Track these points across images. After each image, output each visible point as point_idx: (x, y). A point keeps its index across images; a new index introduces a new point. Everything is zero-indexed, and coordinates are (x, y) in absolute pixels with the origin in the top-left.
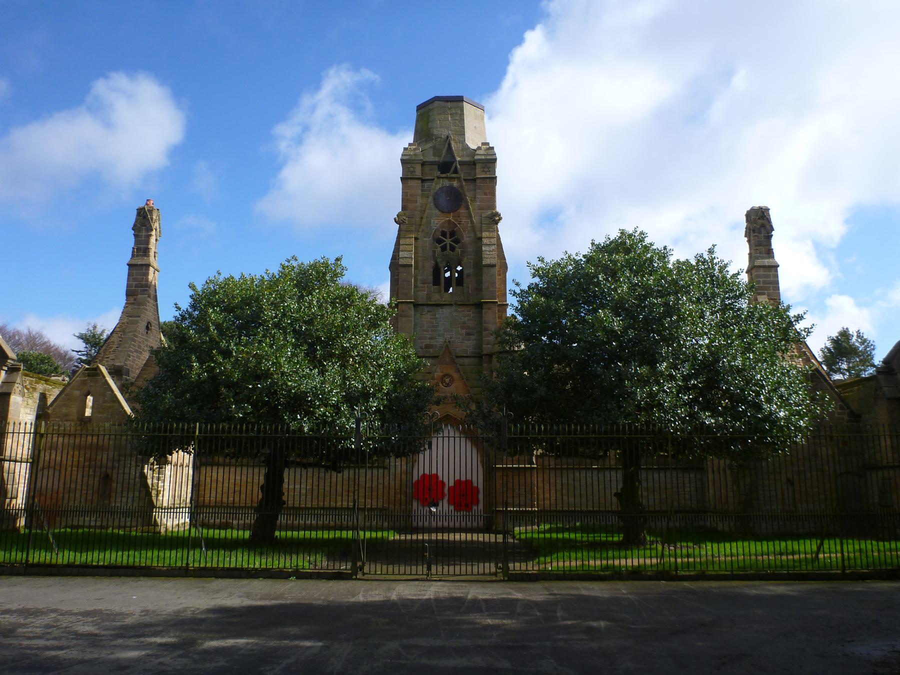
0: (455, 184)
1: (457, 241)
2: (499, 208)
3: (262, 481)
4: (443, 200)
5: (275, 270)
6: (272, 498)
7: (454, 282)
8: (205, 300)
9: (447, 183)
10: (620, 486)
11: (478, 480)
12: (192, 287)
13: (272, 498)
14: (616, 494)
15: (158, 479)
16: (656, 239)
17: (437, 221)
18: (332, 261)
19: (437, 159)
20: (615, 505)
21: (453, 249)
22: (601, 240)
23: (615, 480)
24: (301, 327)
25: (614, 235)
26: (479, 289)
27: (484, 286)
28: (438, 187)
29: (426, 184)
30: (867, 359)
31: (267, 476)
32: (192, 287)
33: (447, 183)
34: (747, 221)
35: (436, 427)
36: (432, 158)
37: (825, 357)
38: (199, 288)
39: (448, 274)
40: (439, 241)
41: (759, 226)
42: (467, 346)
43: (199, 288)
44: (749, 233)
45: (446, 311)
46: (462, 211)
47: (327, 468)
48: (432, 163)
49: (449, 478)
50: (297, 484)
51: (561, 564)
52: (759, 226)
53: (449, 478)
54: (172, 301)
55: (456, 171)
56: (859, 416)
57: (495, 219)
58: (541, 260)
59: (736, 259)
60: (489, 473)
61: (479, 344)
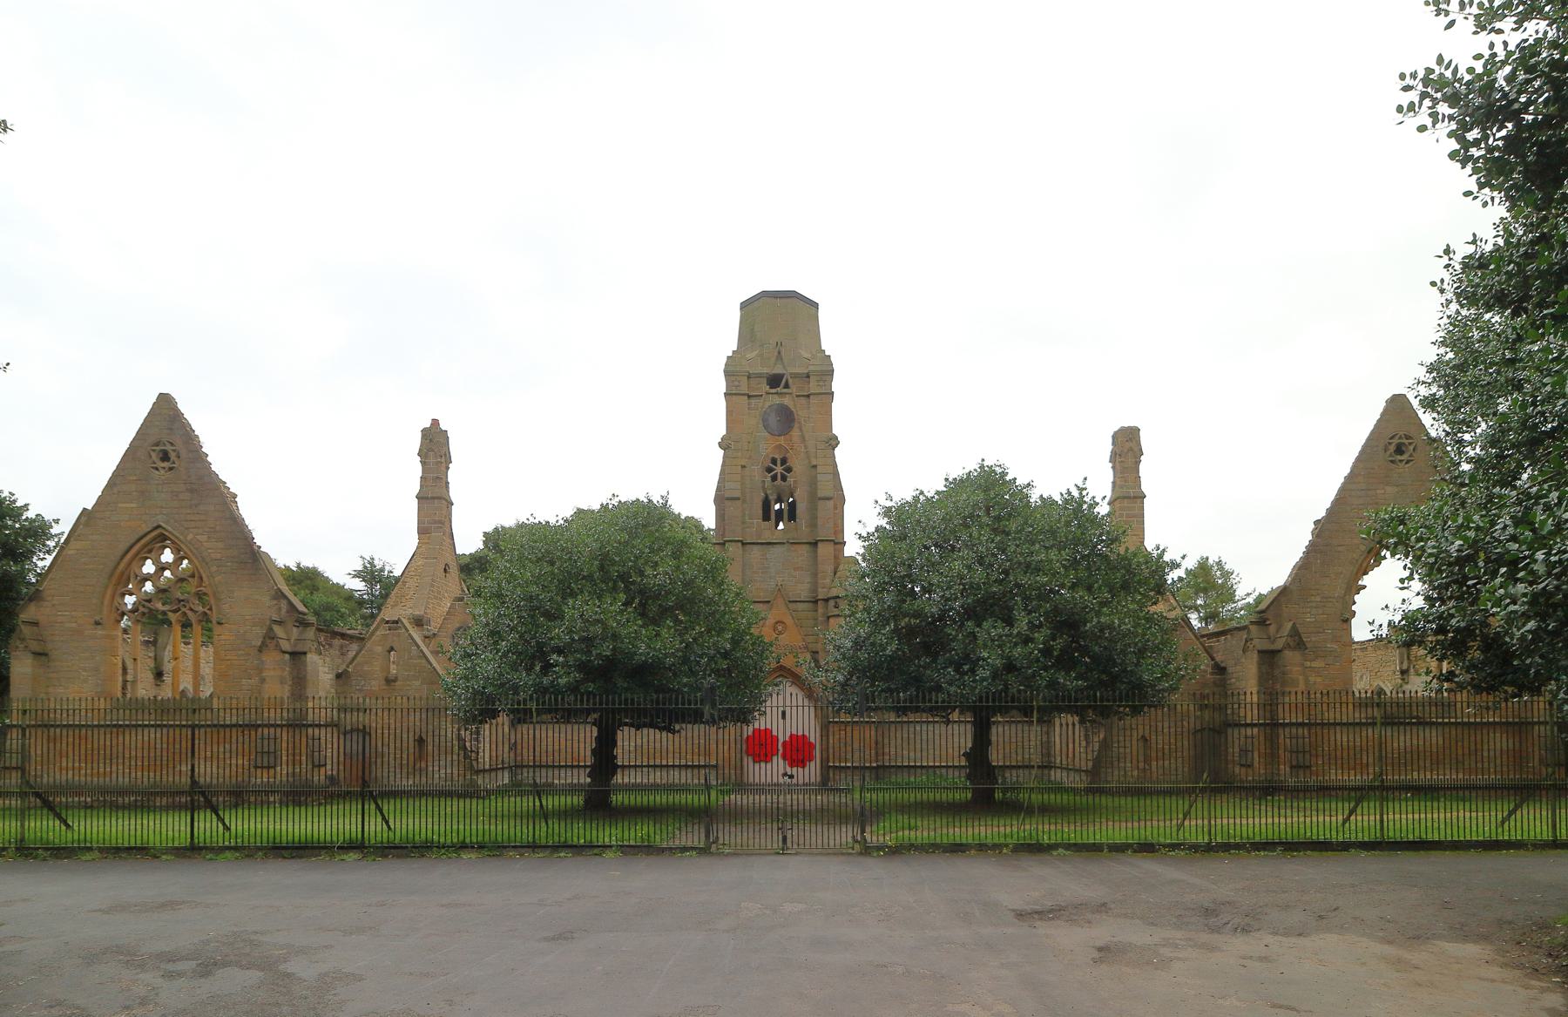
0: (787, 401)
1: (789, 470)
2: (837, 429)
4: (773, 420)
6: (604, 762)
7: (786, 516)
8: (495, 539)
9: (777, 400)
11: (814, 736)
13: (604, 762)
15: (477, 740)
16: (1019, 473)
17: (767, 447)
19: (765, 370)
21: (784, 478)
22: (957, 472)
24: (1122, 622)
25: (972, 465)
26: (813, 525)
27: (820, 522)
28: (768, 404)
29: (753, 401)
30: (1227, 593)
33: (777, 400)
34: (1114, 443)
36: (760, 370)
37: (32, 521)
38: (883, 465)
39: (777, 507)
40: (769, 470)
41: (1127, 448)
42: (802, 590)
43: (883, 465)
44: (1114, 457)
45: (778, 549)
46: (795, 433)
47: (661, 729)
48: (760, 376)
49: (782, 733)
50: (629, 742)
52: (1127, 448)
53: (782, 733)
54: (468, 541)
55: (787, 386)
56: (1224, 669)
57: (833, 442)
59: (1100, 488)
60: (825, 727)
61: (814, 590)
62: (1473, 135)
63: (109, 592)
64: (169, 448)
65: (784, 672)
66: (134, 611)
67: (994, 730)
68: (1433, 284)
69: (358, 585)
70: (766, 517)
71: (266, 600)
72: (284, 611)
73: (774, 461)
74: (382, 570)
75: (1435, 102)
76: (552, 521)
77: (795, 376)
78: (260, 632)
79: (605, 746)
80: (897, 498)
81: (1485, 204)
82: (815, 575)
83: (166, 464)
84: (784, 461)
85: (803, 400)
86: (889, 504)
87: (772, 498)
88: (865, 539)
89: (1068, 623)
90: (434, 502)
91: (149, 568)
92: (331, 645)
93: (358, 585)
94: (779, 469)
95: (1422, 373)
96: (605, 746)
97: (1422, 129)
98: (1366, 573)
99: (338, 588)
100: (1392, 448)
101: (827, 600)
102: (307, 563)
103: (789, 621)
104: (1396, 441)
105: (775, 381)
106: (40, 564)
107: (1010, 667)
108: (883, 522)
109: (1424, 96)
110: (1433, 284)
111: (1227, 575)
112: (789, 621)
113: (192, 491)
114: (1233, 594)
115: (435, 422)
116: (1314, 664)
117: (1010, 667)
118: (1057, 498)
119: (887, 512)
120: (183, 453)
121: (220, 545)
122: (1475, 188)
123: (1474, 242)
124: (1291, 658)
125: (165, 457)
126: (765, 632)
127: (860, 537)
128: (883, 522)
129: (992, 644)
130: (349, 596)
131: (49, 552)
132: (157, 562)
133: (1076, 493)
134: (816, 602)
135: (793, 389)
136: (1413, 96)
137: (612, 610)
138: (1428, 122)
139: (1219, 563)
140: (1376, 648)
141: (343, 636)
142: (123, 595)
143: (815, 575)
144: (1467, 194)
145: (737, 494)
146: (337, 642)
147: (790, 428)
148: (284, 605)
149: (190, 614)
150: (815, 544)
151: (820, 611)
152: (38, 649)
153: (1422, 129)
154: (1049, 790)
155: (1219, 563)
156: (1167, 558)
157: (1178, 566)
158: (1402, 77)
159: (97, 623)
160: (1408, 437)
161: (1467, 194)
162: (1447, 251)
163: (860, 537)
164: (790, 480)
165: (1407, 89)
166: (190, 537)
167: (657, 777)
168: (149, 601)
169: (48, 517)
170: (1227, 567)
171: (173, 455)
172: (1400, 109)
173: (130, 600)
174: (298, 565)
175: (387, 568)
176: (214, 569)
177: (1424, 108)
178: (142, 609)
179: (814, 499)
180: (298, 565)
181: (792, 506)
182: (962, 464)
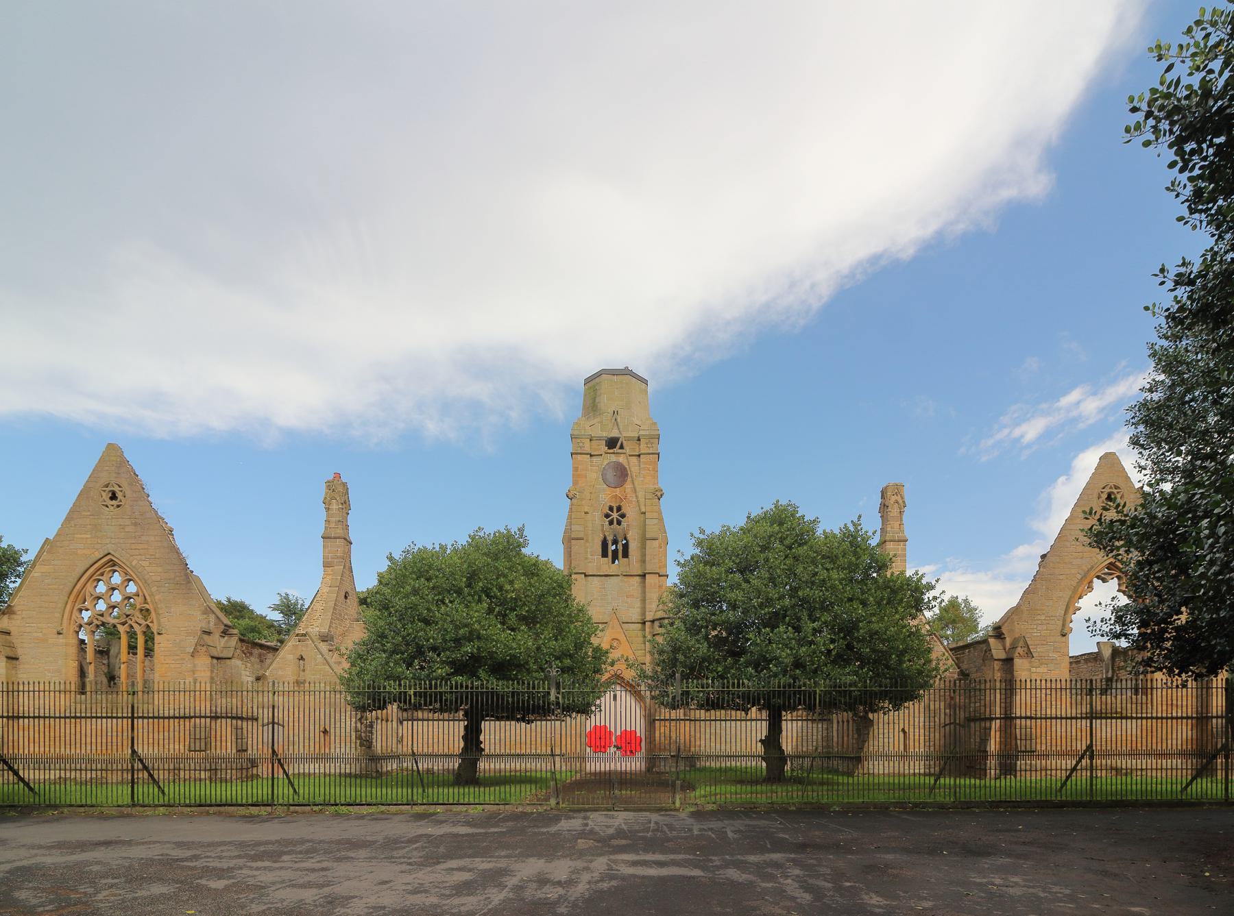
0: (621, 459)
1: (623, 516)
3: (462, 733)
4: (610, 475)
5: (463, 540)
9: (613, 458)
10: (764, 734)
12: (390, 558)
14: (761, 741)
16: (807, 512)
17: (606, 497)
18: (514, 530)
20: (760, 749)
21: (619, 523)
22: (756, 512)
23: (762, 729)
25: (769, 506)
27: (647, 559)
28: (606, 462)
29: (594, 459)
30: (972, 624)
31: (466, 727)
32: (390, 558)
35: (608, 684)
40: (607, 516)
46: (628, 486)
48: (599, 439)
50: (494, 733)
51: (528, 765)
54: (365, 581)
55: (622, 447)
58: (702, 532)
60: (651, 722)
61: (644, 614)
62: (1188, 147)
63: (68, 607)
64: (116, 489)
65: (618, 679)
66: (90, 624)
67: (784, 723)
68: (1147, 308)
69: (276, 616)
70: (605, 554)
71: (198, 614)
72: (212, 624)
73: (611, 509)
74: (296, 604)
75: (1158, 120)
76: (430, 547)
77: (629, 439)
78: (192, 641)
79: (472, 738)
80: (708, 532)
81: (1195, 227)
82: (644, 601)
83: (114, 502)
84: (619, 509)
85: (634, 459)
86: (702, 536)
87: (610, 539)
88: (683, 566)
89: (847, 629)
90: (338, 539)
91: (102, 588)
92: (251, 654)
93: (276, 616)
94: (615, 515)
95: (1108, 614)
96: (472, 738)
97: (1147, 144)
98: (1080, 598)
99: (262, 618)
100: (1105, 496)
101: (653, 621)
102: (237, 598)
103: (622, 638)
104: (1107, 490)
105: (612, 443)
106: (12, 585)
107: (798, 664)
108: (697, 551)
109: (1149, 114)
110: (1147, 308)
111: (972, 610)
112: (622, 638)
113: (136, 524)
114: (976, 626)
115: (338, 476)
116: (1038, 670)
117: (798, 664)
118: (837, 531)
119: (700, 543)
120: (128, 494)
121: (160, 569)
122: (1186, 213)
123: (1184, 264)
124: (1018, 662)
125: (114, 497)
126: (601, 640)
127: (679, 563)
128: (697, 551)
129: (782, 645)
130: (271, 625)
131: (18, 576)
132: (108, 582)
133: (852, 528)
134: (644, 623)
135: (627, 450)
136: (1140, 116)
137: (476, 614)
138: (1153, 137)
139: (966, 601)
140: (1087, 661)
141: (262, 646)
142: (81, 610)
143: (644, 601)
144: (1180, 219)
145: (581, 535)
146: (256, 651)
147: (624, 481)
148: (212, 618)
149: (135, 625)
150: (644, 576)
151: (647, 630)
152: (11, 655)
153: (1147, 144)
154: (829, 772)
155: (966, 601)
156: (924, 582)
157: (933, 588)
158: (1131, 99)
159: (59, 633)
160: (1116, 487)
161: (1180, 219)
162: (1162, 270)
163: (679, 563)
164: (624, 524)
165: (1134, 110)
166: (134, 563)
167: (517, 765)
168: (102, 615)
169: (18, 547)
170: (973, 604)
171: (119, 495)
172: (1128, 130)
173: (86, 615)
174: (229, 600)
175: (300, 602)
176: (154, 589)
177: (1148, 127)
178: (96, 622)
179: (644, 540)
180: (229, 600)
181: (626, 547)
182: (760, 505)
